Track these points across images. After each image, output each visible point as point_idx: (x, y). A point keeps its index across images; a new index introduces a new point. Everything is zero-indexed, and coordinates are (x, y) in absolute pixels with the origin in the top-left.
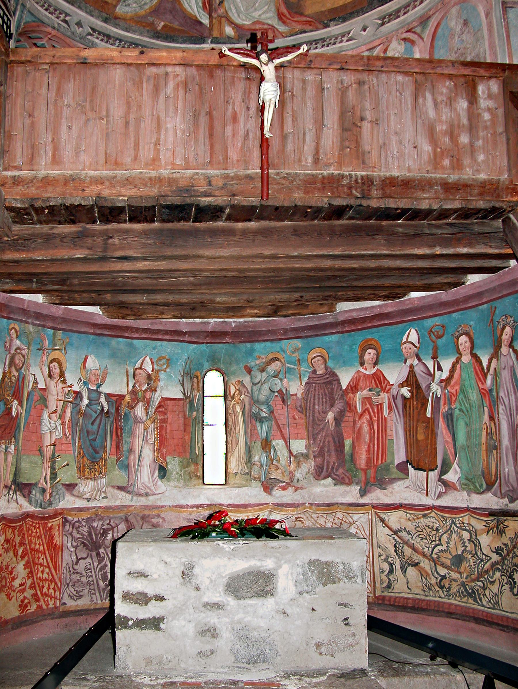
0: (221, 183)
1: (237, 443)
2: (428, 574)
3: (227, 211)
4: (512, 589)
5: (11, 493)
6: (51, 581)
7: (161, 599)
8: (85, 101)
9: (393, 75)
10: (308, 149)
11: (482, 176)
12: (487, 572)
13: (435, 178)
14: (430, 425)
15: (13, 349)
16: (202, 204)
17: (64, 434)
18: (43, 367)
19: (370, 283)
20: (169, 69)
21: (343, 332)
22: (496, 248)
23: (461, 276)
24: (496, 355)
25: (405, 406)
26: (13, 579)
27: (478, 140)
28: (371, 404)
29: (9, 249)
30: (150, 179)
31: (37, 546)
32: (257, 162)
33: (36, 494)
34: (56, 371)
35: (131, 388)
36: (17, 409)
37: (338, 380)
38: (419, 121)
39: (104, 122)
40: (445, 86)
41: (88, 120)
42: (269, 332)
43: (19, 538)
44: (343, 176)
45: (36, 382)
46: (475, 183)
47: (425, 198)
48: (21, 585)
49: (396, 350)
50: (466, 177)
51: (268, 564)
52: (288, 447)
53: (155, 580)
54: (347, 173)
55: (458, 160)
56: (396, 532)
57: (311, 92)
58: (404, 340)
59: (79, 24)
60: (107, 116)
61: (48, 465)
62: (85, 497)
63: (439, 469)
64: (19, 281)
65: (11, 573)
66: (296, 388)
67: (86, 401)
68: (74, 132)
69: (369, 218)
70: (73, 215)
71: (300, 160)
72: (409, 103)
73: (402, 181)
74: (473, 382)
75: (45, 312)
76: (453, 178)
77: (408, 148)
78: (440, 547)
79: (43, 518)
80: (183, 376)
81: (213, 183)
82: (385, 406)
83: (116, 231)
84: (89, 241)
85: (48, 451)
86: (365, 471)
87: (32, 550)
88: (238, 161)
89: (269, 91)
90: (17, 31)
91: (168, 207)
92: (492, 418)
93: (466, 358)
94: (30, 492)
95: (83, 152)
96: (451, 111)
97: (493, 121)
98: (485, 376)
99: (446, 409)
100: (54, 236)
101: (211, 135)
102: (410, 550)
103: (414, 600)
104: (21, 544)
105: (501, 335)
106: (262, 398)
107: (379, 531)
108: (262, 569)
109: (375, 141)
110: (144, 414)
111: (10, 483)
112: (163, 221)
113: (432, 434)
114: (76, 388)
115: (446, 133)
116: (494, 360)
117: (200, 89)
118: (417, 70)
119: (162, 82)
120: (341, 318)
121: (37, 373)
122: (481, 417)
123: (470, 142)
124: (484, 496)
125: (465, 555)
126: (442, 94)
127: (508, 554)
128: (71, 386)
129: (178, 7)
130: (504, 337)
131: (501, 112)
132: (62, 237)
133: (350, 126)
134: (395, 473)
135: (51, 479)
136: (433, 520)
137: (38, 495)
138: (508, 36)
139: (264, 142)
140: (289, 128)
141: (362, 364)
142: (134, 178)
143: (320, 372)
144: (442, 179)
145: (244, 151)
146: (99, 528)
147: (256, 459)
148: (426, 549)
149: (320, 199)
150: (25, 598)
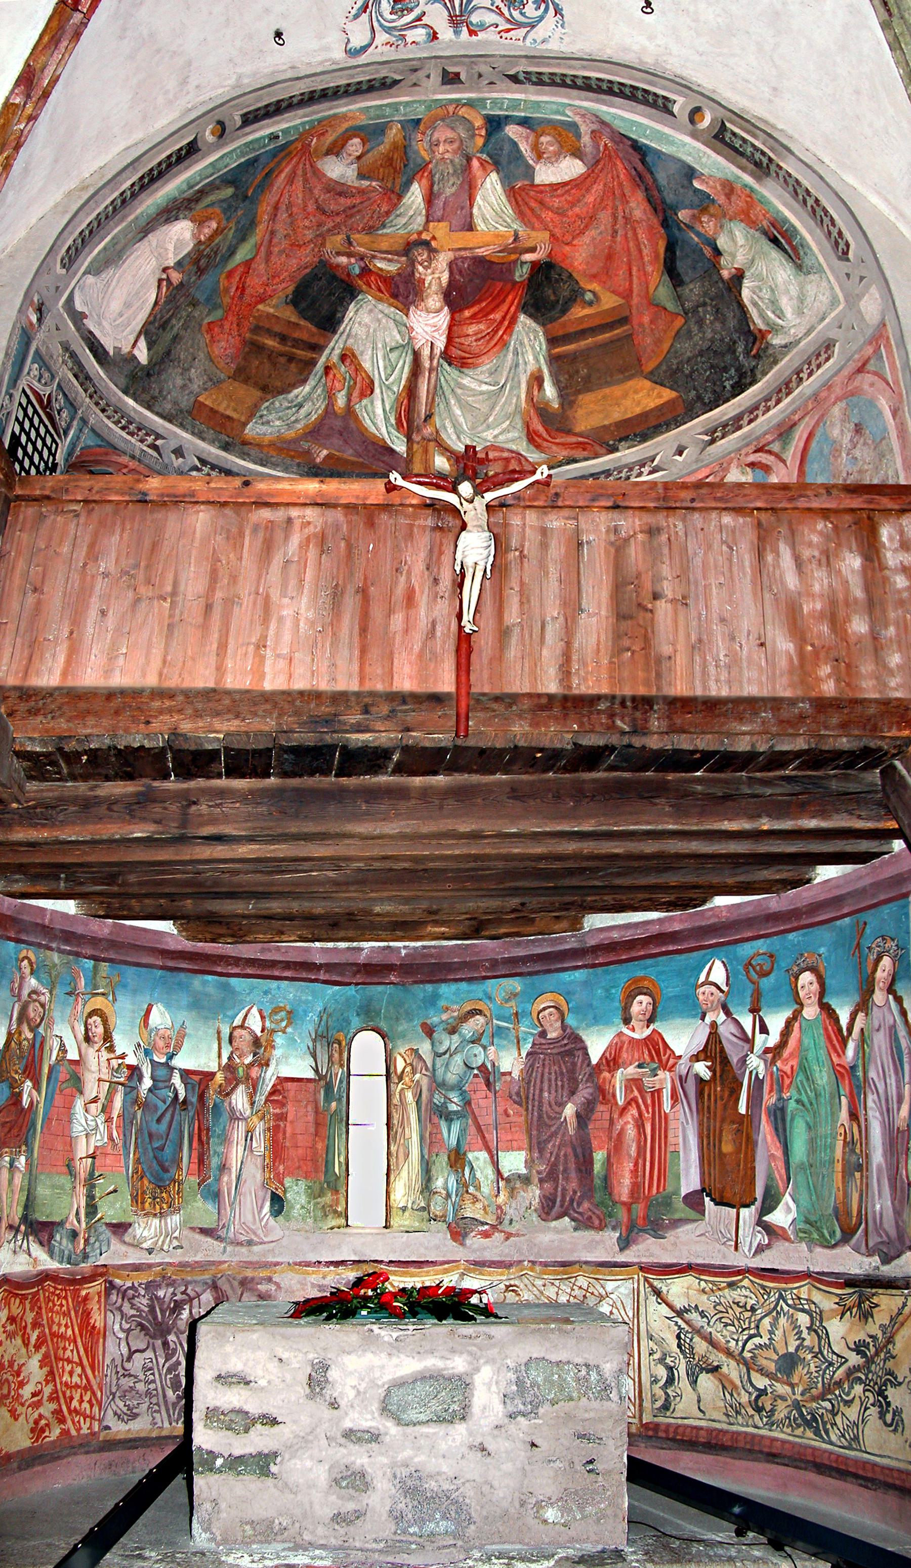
1: (407, 1156)
2: (735, 1387)
3: (395, 757)
4: (882, 1415)
5: (19, 1237)
6: (86, 1389)
7: (274, 1422)
12: (839, 1384)
14: (745, 1129)
15: (25, 992)
16: (352, 745)
17: (111, 1138)
20: (294, 512)
21: (594, 966)
22: (868, 819)
23: (804, 869)
24: (863, 1006)
25: (700, 1094)
26: (21, 1384)
29: (20, 824)
31: (63, 1329)
33: (61, 1240)
35: (225, 1060)
36: (30, 1095)
43: (33, 1315)
45: (63, 1049)
48: (34, 1395)
49: (687, 997)
51: (459, 1364)
52: (495, 1163)
53: (262, 1389)
56: (680, 1313)
58: (702, 978)
59: (179, 452)
61: (82, 1191)
62: (145, 1245)
63: (758, 1203)
66: (510, 1061)
67: (147, 1083)
74: (823, 1053)
75: (80, 930)
78: (757, 1340)
79: (73, 1282)
80: (314, 1041)
83: (204, 791)
86: (628, 1206)
87: (53, 1335)
89: (474, 548)
92: (853, 1116)
93: (811, 1012)
94: (51, 1237)
98: (844, 1042)
99: (773, 1100)
100: (96, 802)
103: (710, 1431)
104: (36, 1325)
105: (875, 970)
106: (451, 1078)
110: (247, 1106)
111: (17, 1221)
112: (285, 775)
114: (131, 1060)
116: (861, 1015)
117: (349, 547)
119: (279, 535)
120: (592, 942)
121: (65, 1035)
122: (834, 1115)
124: (837, 1251)
125: (801, 1354)
127: (877, 1354)
129: (353, 425)
130: (879, 974)
132: (111, 803)
134: (681, 1210)
135: (87, 1215)
136: (746, 1292)
137: (64, 1242)
140: (512, 616)
141: (627, 1021)
143: (552, 1035)
147: (439, 1183)
148: (733, 1343)
150: (40, 1416)
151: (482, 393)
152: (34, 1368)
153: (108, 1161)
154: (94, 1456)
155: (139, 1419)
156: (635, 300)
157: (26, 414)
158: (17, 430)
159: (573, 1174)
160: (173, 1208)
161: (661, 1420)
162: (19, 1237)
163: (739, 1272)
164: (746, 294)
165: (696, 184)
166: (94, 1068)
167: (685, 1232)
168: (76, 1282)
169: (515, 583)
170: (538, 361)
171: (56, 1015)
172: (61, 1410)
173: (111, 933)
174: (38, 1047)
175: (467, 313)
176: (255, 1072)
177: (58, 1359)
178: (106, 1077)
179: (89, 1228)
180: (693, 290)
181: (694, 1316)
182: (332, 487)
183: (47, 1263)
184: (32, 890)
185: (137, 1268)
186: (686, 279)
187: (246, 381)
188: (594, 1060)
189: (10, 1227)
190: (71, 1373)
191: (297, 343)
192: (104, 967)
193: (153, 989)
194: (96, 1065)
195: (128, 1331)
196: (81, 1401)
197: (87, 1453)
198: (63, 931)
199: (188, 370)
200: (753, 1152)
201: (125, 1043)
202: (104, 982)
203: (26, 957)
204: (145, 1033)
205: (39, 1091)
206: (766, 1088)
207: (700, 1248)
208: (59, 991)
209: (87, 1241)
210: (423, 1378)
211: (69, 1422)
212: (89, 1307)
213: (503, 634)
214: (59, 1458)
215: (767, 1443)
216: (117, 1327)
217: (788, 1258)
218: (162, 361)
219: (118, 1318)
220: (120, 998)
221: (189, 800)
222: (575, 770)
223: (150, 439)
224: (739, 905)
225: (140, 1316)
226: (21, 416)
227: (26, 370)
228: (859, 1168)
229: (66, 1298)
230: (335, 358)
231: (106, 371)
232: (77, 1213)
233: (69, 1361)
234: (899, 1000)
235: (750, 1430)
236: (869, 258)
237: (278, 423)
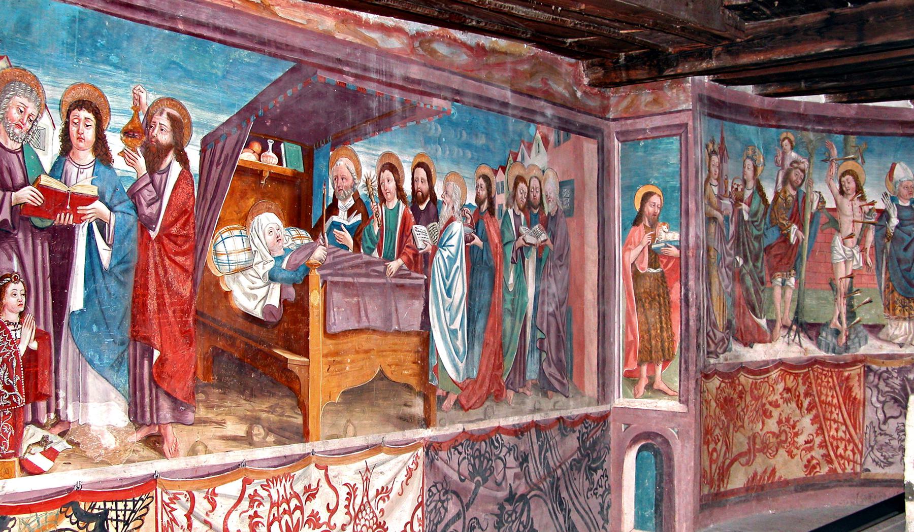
17: (865, 263)
26: (796, 434)
29: (744, 52)
31: (830, 399)
36: (796, 234)
45: (822, 201)
48: (806, 442)
62: (896, 341)
67: (895, 221)
75: (830, 113)
79: (838, 366)
87: (821, 402)
94: (818, 334)
104: (807, 394)
114: (880, 205)
121: (823, 191)
135: (847, 319)
137: (830, 338)
152: (806, 423)
153: (863, 280)
154: (857, 489)
155: (893, 466)
162: (792, 334)
168: (839, 366)
171: (815, 176)
172: (829, 455)
173: (857, 113)
174: (801, 201)
177: (825, 419)
178: (859, 219)
179: (849, 328)
183: (814, 351)
184: (782, 91)
185: (890, 357)
189: (784, 327)
190: (837, 430)
192: (853, 139)
193: (896, 151)
194: (850, 211)
195: (884, 403)
196: (846, 449)
197: (851, 486)
198: (816, 116)
201: (875, 195)
202: (853, 150)
203: (787, 138)
204: (891, 185)
205: (804, 233)
208: (816, 159)
209: (848, 337)
212: (851, 384)
214: (828, 487)
216: (874, 399)
219: (875, 393)
220: (867, 160)
225: (894, 392)
229: (831, 377)
232: (839, 317)
233: (835, 421)
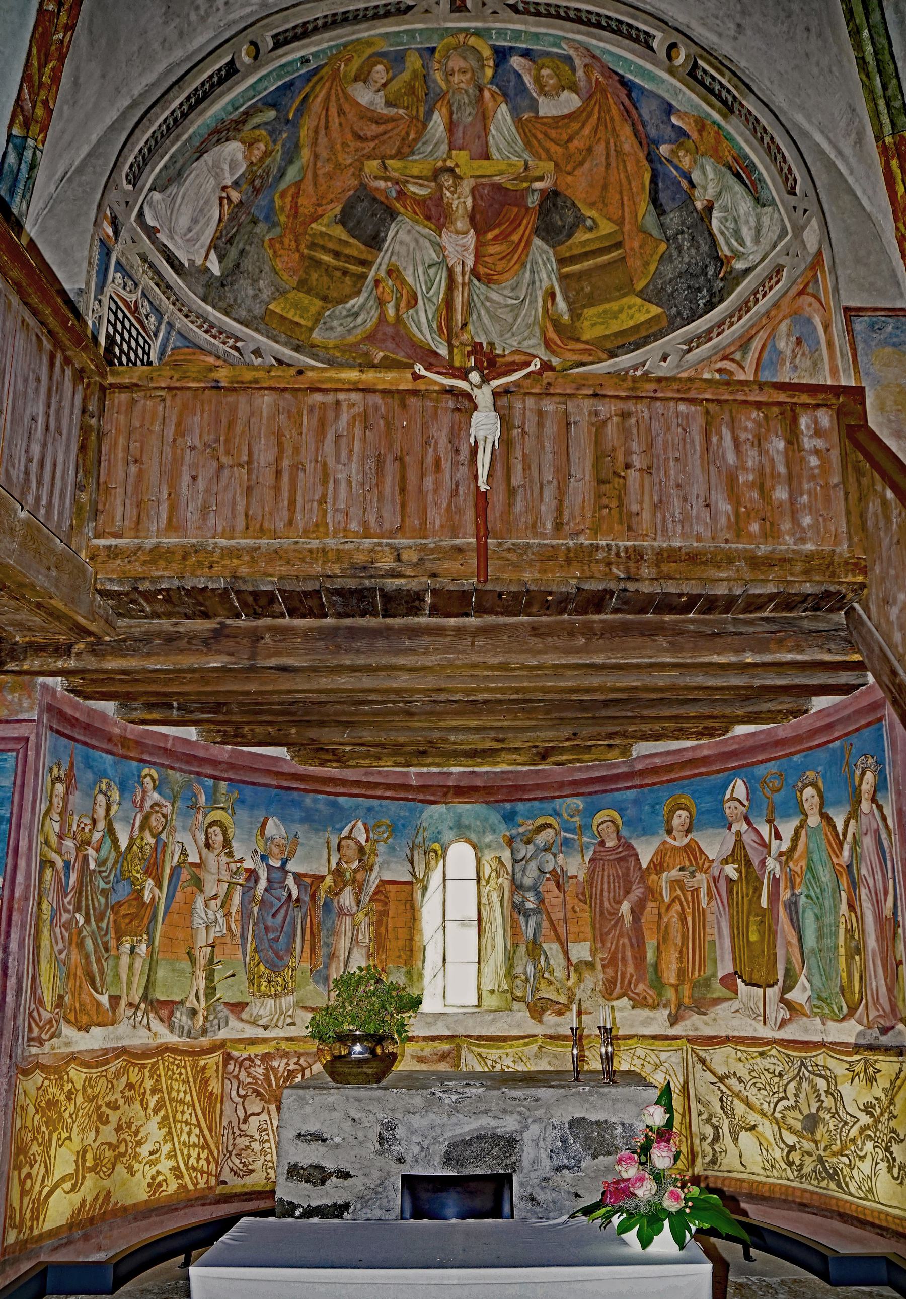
0: (414, 557)
1: (494, 946)
2: (770, 1144)
3: (428, 600)
4: (890, 1169)
5: (140, 1014)
6: (203, 1148)
7: (347, 1176)
8: (217, 440)
9: (672, 404)
10: (547, 509)
11: (810, 547)
12: (853, 1141)
13: (737, 550)
14: (767, 919)
15: (148, 805)
16: (387, 588)
17: (230, 930)
18: (197, 834)
19: (667, 713)
20: (342, 396)
21: (641, 786)
22: (837, 652)
23: (802, 701)
24: (854, 814)
25: (730, 892)
26: (139, 1144)
27: (802, 495)
28: (682, 889)
29: (112, 654)
30: (310, 551)
31: (181, 1095)
32: (470, 527)
33: (181, 1017)
34: (218, 838)
35: (334, 865)
36: (152, 891)
37: (637, 855)
38: (712, 468)
39: (245, 471)
40: (749, 419)
41: (220, 468)
42: (538, 787)
43: (152, 1082)
44: (597, 548)
45: (184, 852)
46: (797, 557)
47: (722, 580)
48: (151, 1153)
49: (716, 810)
50: (783, 547)
51: (509, 1125)
52: (566, 953)
53: (337, 1146)
54: (604, 543)
55: (772, 524)
56: (722, 1079)
57: (551, 428)
58: (728, 795)
59: (257, 353)
60: (249, 462)
61: (201, 975)
62: (260, 1022)
63: (780, 984)
64: (150, 706)
65: (136, 1134)
66: (575, 866)
67: (263, 883)
68: (201, 484)
69: (643, 611)
70: (201, 605)
71: (534, 525)
72: (697, 443)
73: (687, 554)
74: (825, 855)
75: (201, 753)
76: (764, 550)
77: (696, 508)
78: (785, 1103)
79: (192, 1053)
80: (412, 850)
81: (404, 557)
82: (703, 892)
83: (270, 629)
84: (230, 644)
85: (203, 956)
86: (676, 987)
87: (171, 1100)
88: (442, 526)
89: (485, 426)
90: (160, 359)
91: (338, 592)
92: (851, 907)
93: (814, 820)
94: (171, 1014)
95: (212, 514)
96: (760, 454)
97: (825, 467)
98: (841, 845)
99: (788, 896)
100: (178, 636)
101: (403, 490)
102: (743, 1106)
103: (752, 1183)
104: (154, 1091)
105: (861, 784)
106: (528, 881)
107: (697, 1076)
108: (499, 1132)
109: (647, 498)
110: (353, 904)
111: (137, 1000)
112: (340, 615)
113: (770, 933)
114: (249, 864)
115: (751, 486)
116: (852, 822)
117: (388, 424)
118: (708, 396)
119: (331, 415)
120: (639, 767)
121: (186, 843)
122: (836, 907)
123: (791, 497)
124: (845, 1024)
125: (822, 1114)
126: (746, 429)
127: (882, 1114)
128: (241, 861)
129: (402, 332)
130: (864, 787)
131: (835, 455)
132: (191, 638)
133: (608, 476)
134: (718, 990)
135: (207, 996)
136: (774, 1061)
137: (184, 1018)
138: (855, 356)
139: (482, 499)
140: (517, 479)
141: (669, 832)
142: (286, 551)
143: (609, 844)
144: (746, 550)
145: (452, 510)
146: (281, 1069)
147: (519, 970)
148: (765, 1105)
149: (564, 580)
150: (158, 1172)
151: (507, 306)
156: (627, 227)
157: (117, 318)
158: (111, 331)
159: (630, 961)
160: (287, 990)
161: (709, 1173)
163: (768, 1043)
164: (715, 224)
165: (674, 120)
166: (214, 869)
167: (722, 1010)
169: (518, 454)
170: (550, 279)
175: (490, 235)
176: (360, 876)
180: (674, 219)
181: (733, 1082)
182: (369, 376)
185: (253, 1042)
186: (668, 209)
187: (308, 292)
188: (644, 865)
191: (349, 259)
192: (223, 785)
199: (257, 281)
200: (775, 941)
205: (160, 888)
206: (782, 885)
207: (735, 1022)
210: (479, 1138)
211: (187, 1177)
212: (207, 1075)
213: (511, 492)
215: (798, 1193)
216: (234, 1093)
217: (806, 1030)
218: (233, 273)
221: (256, 637)
222: (586, 613)
223: (231, 342)
224: (753, 734)
226: (112, 319)
227: (110, 278)
228: (858, 951)
230: (382, 274)
231: (184, 281)
234: (880, 808)
235: (784, 1182)
236: (811, 193)
237: (339, 329)
